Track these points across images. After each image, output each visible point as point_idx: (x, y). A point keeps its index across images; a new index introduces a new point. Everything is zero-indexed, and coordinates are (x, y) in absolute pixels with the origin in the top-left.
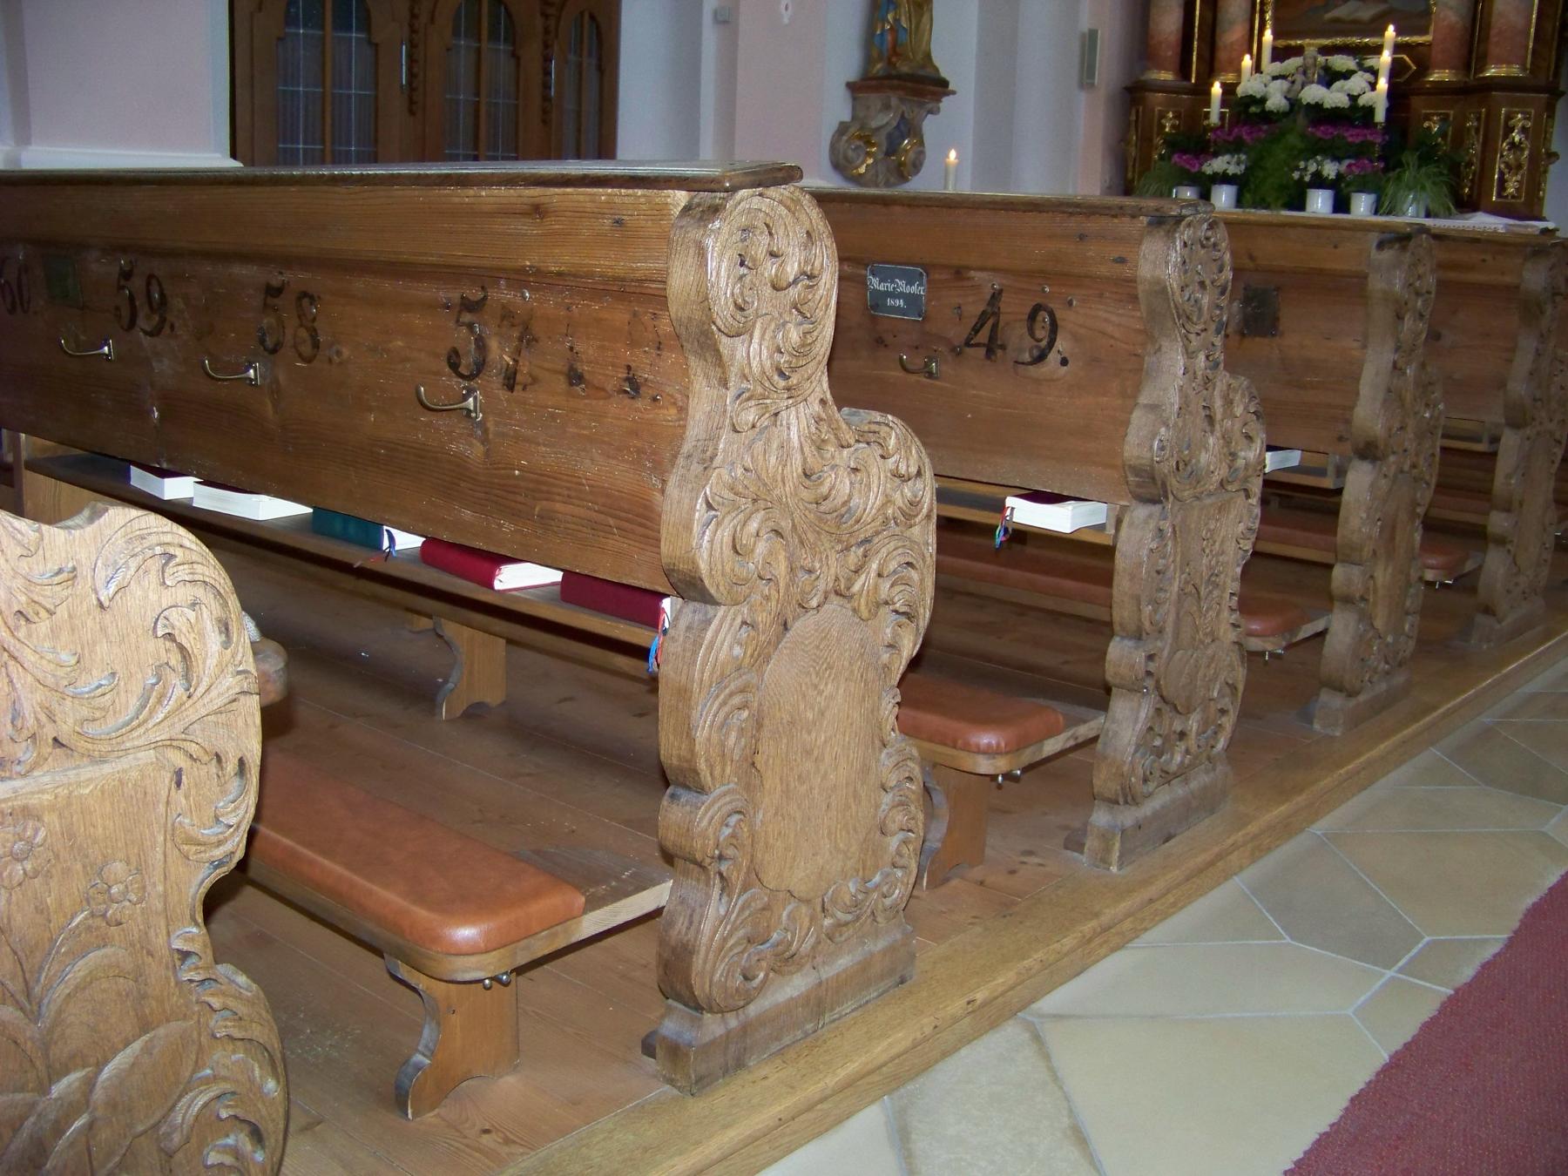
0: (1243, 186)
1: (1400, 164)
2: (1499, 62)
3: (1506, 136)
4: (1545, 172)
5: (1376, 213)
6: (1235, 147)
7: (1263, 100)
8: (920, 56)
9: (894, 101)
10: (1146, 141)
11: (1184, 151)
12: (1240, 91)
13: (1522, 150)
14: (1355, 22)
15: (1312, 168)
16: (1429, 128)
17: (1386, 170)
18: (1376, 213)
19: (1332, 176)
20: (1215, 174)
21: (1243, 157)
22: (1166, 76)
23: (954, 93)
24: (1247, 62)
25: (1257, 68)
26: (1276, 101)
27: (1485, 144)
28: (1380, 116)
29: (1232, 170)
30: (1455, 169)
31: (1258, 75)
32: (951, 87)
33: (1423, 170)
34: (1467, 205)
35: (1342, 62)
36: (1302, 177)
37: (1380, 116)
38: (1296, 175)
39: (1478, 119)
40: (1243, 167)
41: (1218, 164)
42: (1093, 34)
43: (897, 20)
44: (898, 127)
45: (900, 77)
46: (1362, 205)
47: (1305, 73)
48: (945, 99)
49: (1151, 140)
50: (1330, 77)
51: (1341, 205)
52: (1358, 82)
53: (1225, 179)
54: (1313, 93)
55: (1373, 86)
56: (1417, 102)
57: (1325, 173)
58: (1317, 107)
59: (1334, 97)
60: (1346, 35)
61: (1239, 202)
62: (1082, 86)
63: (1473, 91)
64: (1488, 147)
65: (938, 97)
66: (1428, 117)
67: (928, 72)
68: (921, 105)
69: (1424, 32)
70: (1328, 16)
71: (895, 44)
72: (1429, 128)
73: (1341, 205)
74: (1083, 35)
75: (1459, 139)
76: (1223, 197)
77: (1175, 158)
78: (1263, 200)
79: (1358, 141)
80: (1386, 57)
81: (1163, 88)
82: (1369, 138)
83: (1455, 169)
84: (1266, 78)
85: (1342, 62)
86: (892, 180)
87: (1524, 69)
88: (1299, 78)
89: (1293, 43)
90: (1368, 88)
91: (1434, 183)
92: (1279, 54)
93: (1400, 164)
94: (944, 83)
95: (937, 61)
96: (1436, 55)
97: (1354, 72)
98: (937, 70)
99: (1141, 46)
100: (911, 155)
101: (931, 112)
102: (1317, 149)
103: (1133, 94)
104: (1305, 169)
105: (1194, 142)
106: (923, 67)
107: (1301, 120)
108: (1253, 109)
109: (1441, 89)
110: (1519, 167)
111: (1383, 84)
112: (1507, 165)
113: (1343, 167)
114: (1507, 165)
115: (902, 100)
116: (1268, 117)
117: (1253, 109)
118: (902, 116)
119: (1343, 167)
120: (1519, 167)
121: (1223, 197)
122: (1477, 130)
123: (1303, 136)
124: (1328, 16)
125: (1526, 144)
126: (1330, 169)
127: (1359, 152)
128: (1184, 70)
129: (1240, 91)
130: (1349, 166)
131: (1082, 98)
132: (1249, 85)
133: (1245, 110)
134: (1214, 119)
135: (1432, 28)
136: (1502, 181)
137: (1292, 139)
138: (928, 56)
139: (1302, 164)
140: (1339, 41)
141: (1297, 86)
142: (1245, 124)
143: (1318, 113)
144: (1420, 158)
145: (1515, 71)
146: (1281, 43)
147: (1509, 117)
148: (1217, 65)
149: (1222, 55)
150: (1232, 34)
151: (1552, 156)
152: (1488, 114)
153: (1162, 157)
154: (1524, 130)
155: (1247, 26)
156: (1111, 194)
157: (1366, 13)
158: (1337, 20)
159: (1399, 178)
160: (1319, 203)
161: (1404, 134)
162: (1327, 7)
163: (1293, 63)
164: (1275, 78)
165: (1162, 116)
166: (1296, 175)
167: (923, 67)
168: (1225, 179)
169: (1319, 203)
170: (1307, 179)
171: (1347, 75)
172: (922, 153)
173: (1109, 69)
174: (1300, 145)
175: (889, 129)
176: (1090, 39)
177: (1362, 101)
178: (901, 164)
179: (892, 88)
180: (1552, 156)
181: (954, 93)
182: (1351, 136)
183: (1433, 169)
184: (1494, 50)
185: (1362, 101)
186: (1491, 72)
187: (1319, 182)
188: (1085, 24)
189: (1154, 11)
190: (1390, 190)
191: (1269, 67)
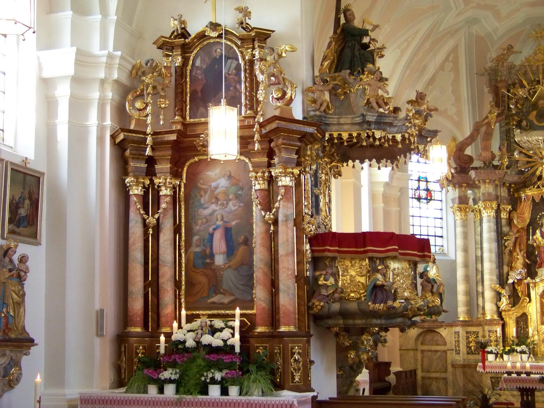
0: (179, 384)
1: (248, 371)
2: (286, 325)
3: (292, 357)
4: (310, 369)
5: (240, 395)
6: (174, 365)
7: (184, 342)
8: (20, 328)
9: (8, 352)
10: (130, 361)
11: (148, 367)
12: (174, 338)
13: (299, 362)
14: (222, 304)
15: (210, 375)
16: (259, 352)
17: (242, 375)
18: (240, 395)
19: (219, 379)
20: (166, 379)
21: (178, 371)
22: (139, 330)
23: (37, 345)
24: (175, 325)
25: (180, 327)
26: (190, 343)
27: (284, 359)
28: (237, 350)
29: (173, 377)
30: (273, 373)
31: (183, 333)
32: (35, 342)
33: (259, 373)
34: (279, 387)
35: (218, 323)
36: (205, 379)
37: (237, 350)
38: (203, 379)
39: (280, 349)
40: (178, 375)
41: (167, 374)
42: (102, 311)
43: (8, 312)
44: (9, 363)
45: (10, 340)
46: (234, 391)
47: (202, 329)
48: (32, 348)
49: (133, 360)
50: (213, 331)
51: (225, 392)
52: (226, 333)
53: (170, 381)
54: (207, 339)
55: (233, 335)
56: (252, 340)
57: (216, 378)
58: (210, 345)
59: (216, 341)
60: (185, 210)
61: (177, 392)
62: (97, 335)
63: (275, 336)
64: (285, 361)
65: (29, 348)
66: (257, 348)
67: (24, 336)
68: (20, 352)
69: (253, 309)
70: (209, 301)
71: (7, 324)
72: (259, 352)
73: (225, 392)
74: (97, 312)
75: (272, 356)
76: (170, 390)
77: (146, 371)
78: (189, 390)
79: (229, 361)
80: (237, 324)
81: (137, 335)
82: (234, 360)
83: (273, 373)
84: (184, 331)
85: (218, 323)
86: (6, 389)
87: (296, 328)
88: (200, 332)
89: (194, 313)
90: (231, 336)
91: (264, 379)
92: (190, 319)
93: (248, 371)
94: (32, 341)
95: (28, 329)
96: (258, 320)
97: (224, 328)
98: (28, 334)
99: (125, 317)
100: (16, 375)
101: (25, 354)
102: (210, 366)
103: (121, 339)
104: (207, 376)
105: (154, 363)
106: (21, 334)
107: (203, 353)
108: (180, 346)
109: (262, 335)
110: (299, 369)
111: (237, 336)
112: (294, 369)
113: (223, 374)
114: (294, 369)
115: (11, 351)
116: (187, 350)
117: (180, 346)
118: (12, 358)
119: (223, 374)
120: (299, 369)
121: (170, 390)
122: (280, 354)
123: (204, 359)
124: (209, 301)
125: (301, 359)
126: (218, 376)
127: (230, 366)
128: (145, 326)
129: (174, 338)
130: (226, 374)
131: (97, 341)
132: (178, 335)
133: (177, 348)
134: (162, 351)
135: (255, 307)
136: (293, 376)
137: (200, 362)
138: (24, 328)
139: (205, 374)
140: (215, 312)
141: (199, 336)
142: (177, 353)
143: (211, 349)
144: (257, 367)
145: (292, 329)
146: (190, 313)
147: (292, 348)
148: (161, 324)
149: (163, 319)
150: (167, 309)
151: (312, 362)
152: (283, 347)
153: (139, 369)
154: (299, 353)
155: (173, 306)
156: (114, 388)
157: (226, 300)
158: (214, 303)
159: (249, 378)
160: (215, 391)
161: (248, 355)
162: (209, 297)
163: (196, 324)
164: (189, 331)
165: (137, 348)
166: (203, 379)
167: (21, 334)
168: (170, 381)
169: (215, 391)
170: (208, 381)
171: (221, 330)
172: (21, 374)
173: (111, 326)
174: (203, 364)
175: (5, 365)
176: (101, 314)
177: (229, 343)
178: (10, 381)
179: (6, 346)
180: (312, 362)
181: (37, 345)
182: (227, 359)
183: (263, 373)
184: (282, 320)
185: (229, 343)
186: (283, 329)
187: (213, 381)
188: (97, 307)
189: (130, 300)
190: (246, 383)
191: (186, 326)
